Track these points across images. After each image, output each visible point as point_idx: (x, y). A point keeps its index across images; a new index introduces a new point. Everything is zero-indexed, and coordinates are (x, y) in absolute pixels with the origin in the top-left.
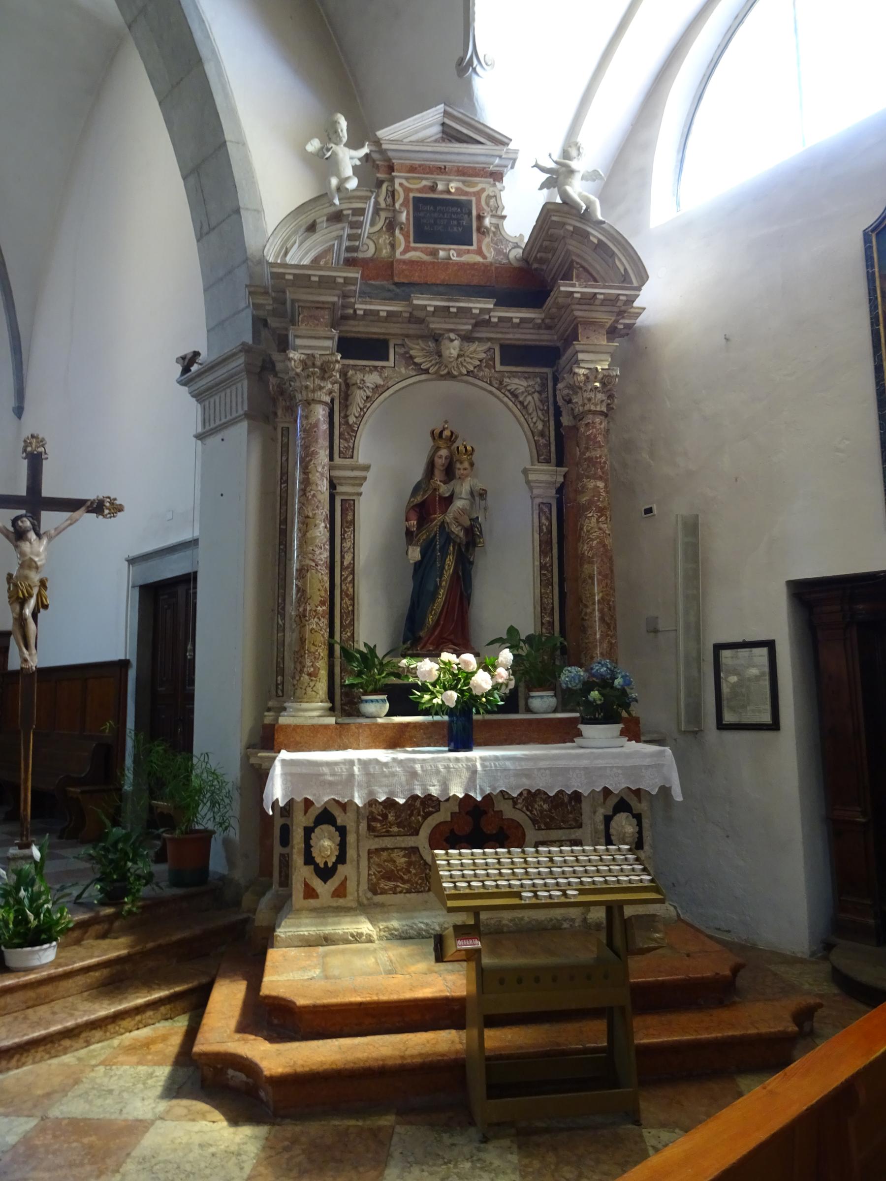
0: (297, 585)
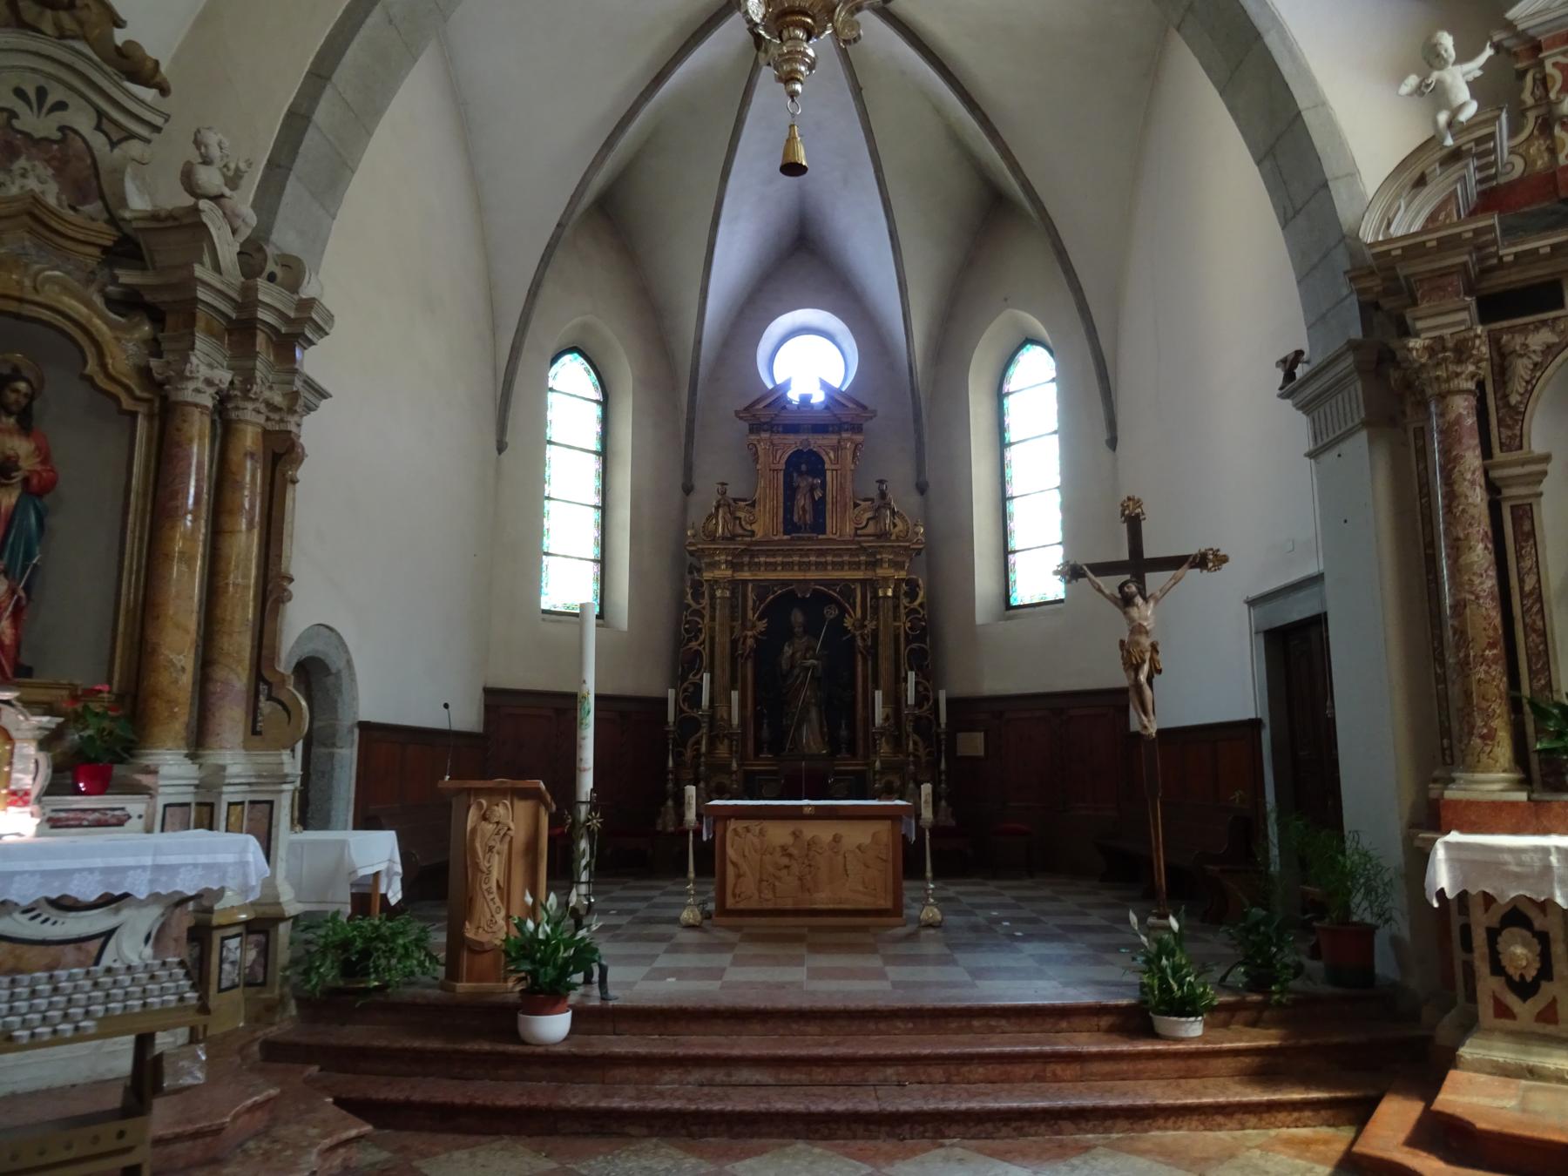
0: (1452, 626)
